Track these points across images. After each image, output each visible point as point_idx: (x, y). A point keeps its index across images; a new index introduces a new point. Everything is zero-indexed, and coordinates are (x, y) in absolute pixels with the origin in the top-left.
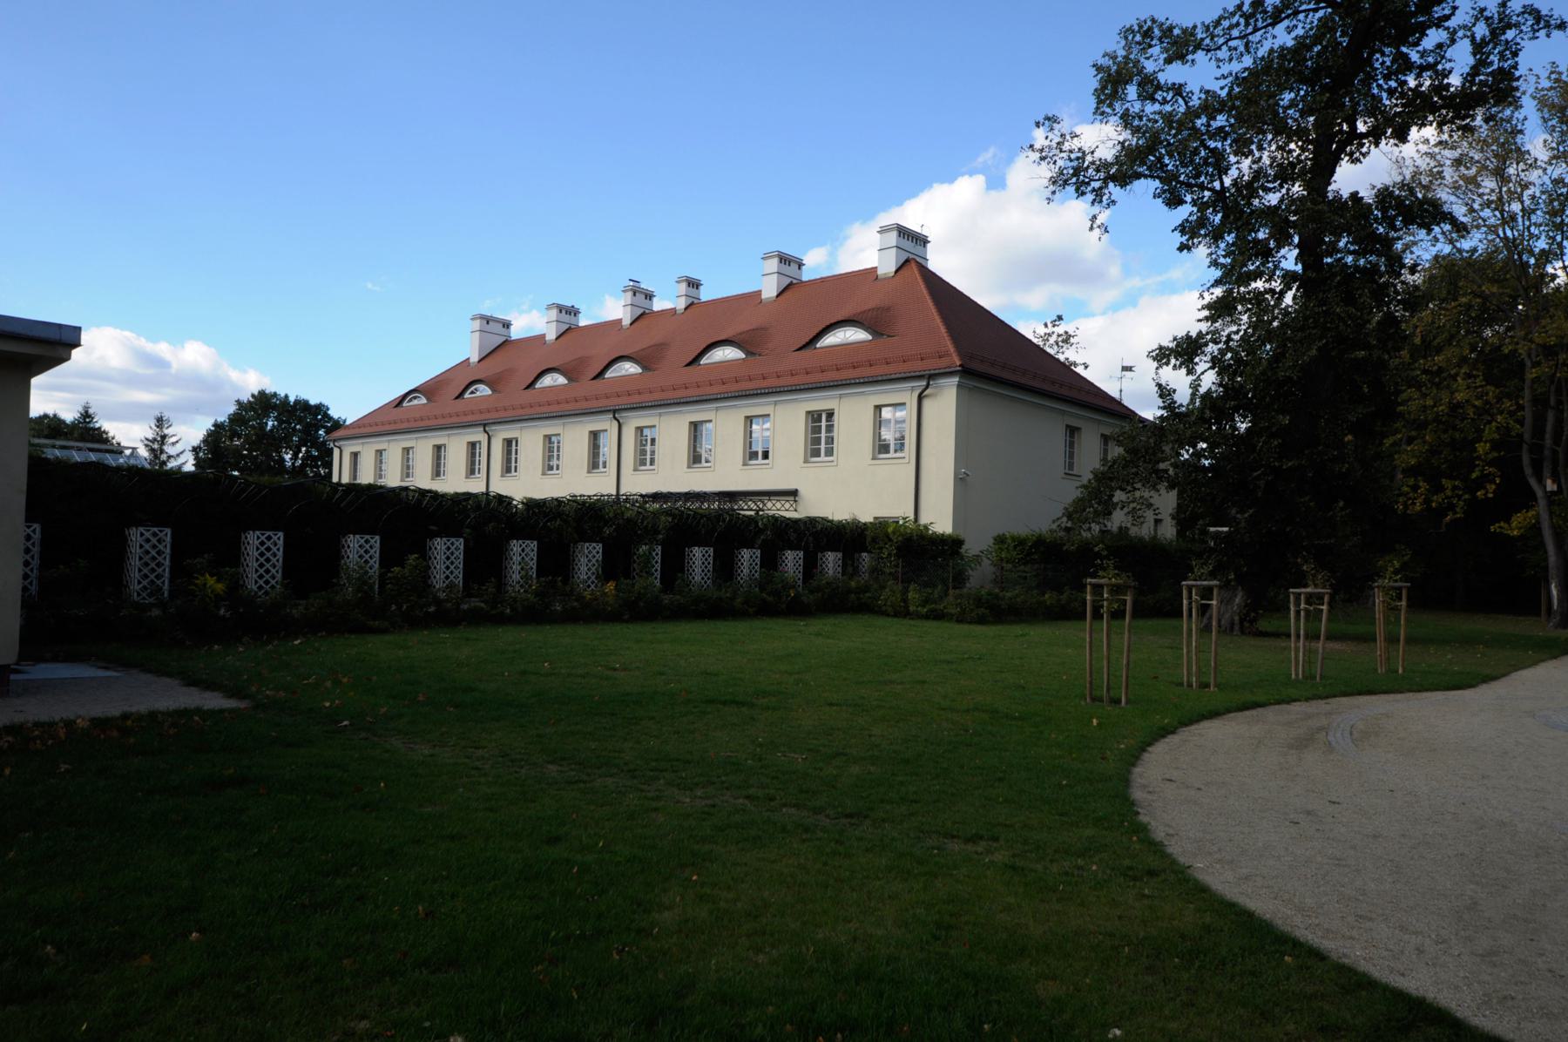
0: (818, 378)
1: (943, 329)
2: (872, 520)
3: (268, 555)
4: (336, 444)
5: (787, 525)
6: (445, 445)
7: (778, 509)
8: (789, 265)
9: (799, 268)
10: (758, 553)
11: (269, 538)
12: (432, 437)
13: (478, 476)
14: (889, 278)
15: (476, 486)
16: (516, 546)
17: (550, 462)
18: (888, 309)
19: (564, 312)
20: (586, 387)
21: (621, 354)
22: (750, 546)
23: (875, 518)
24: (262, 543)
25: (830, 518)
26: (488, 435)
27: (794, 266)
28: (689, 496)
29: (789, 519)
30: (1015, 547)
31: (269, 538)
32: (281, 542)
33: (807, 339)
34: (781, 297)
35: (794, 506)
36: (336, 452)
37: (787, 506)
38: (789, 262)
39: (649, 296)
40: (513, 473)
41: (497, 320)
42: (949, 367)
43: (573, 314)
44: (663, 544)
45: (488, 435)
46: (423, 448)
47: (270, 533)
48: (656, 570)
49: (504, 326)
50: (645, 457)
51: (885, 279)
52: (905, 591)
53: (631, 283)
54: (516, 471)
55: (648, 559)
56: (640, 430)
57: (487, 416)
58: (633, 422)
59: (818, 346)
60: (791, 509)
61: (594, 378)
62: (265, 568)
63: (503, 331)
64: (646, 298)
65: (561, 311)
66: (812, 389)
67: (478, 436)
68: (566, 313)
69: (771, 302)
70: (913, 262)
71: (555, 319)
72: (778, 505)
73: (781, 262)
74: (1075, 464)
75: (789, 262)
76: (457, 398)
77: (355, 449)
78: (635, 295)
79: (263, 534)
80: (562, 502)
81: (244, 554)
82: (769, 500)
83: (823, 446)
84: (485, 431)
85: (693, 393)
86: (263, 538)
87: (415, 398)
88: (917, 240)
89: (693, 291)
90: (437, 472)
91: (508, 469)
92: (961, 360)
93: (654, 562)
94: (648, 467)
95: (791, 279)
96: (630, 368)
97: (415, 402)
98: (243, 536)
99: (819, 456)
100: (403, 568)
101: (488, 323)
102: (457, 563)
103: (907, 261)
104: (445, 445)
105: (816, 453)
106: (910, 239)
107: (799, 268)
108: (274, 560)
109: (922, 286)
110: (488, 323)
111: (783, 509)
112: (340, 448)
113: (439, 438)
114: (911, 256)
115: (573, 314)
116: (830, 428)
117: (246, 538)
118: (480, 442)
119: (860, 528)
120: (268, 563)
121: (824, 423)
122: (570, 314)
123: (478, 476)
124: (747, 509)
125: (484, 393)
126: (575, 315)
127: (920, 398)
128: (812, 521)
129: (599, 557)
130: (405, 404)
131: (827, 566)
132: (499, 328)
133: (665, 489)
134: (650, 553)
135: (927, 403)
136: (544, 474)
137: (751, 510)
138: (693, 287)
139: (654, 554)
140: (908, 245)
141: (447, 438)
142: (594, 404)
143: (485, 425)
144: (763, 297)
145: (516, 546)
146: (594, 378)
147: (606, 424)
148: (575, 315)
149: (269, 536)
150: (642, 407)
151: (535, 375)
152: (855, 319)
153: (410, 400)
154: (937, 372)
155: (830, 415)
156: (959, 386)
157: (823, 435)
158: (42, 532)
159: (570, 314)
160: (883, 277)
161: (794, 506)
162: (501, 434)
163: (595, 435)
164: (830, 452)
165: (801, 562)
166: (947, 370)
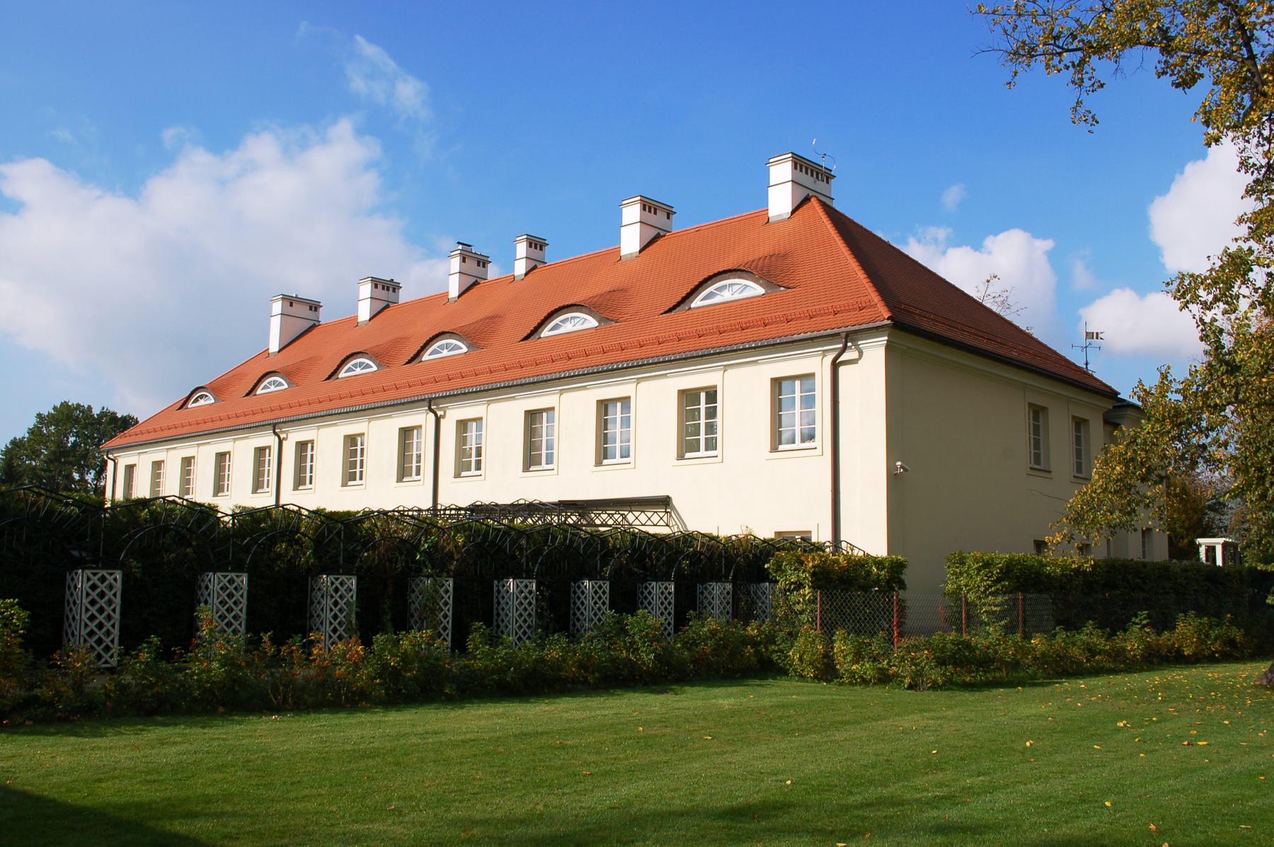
0: (712, 341)
1: (861, 275)
2: (772, 536)
3: (102, 602)
4: (110, 456)
5: (649, 543)
6: (312, 442)
7: (651, 524)
8: (655, 213)
9: (668, 218)
10: (606, 586)
11: (103, 579)
12: (594, 386)
13: (310, 486)
14: (783, 221)
15: (264, 500)
16: (215, 581)
17: (352, 472)
18: (785, 256)
19: (380, 287)
20: (400, 372)
21: (441, 331)
22: (718, 578)
23: (778, 533)
24: (94, 587)
25: (715, 534)
26: (436, 415)
27: (661, 216)
28: (515, 509)
29: (653, 536)
30: (979, 569)
31: (103, 579)
32: (119, 585)
33: (679, 299)
34: (797, 213)
35: (665, 518)
36: (110, 464)
37: (655, 518)
38: (655, 210)
39: (483, 262)
40: (308, 486)
41: (302, 301)
42: (874, 321)
43: (391, 289)
44: (457, 576)
45: (436, 415)
46: (204, 454)
47: (104, 572)
48: (445, 616)
49: (311, 309)
50: (468, 461)
51: (778, 222)
52: (830, 643)
53: (460, 247)
54: (311, 483)
55: (434, 598)
56: (462, 425)
57: (278, 413)
58: (454, 414)
59: (693, 305)
60: (661, 523)
61: (409, 362)
62: (97, 622)
63: (311, 314)
64: (479, 265)
65: (376, 286)
66: (685, 359)
67: (268, 439)
68: (383, 289)
69: (632, 258)
70: (813, 199)
71: (790, 179)
72: (643, 518)
73: (644, 209)
74: (1041, 441)
75: (655, 210)
76: (248, 395)
77: (130, 461)
78: (464, 260)
79: (95, 574)
80: (392, 517)
81: (69, 603)
82: (631, 511)
83: (702, 437)
84: (275, 433)
85: (530, 374)
86: (95, 579)
87: (201, 397)
88: (817, 174)
89: (536, 253)
90: (219, 488)
91: (299, 482)
92: (890, 310)
93: (441, 604)
94: (358, 482)
95: (657, 231)
96: (581, 322)
97: (202, 402)
98: (69, 578)
99: (355, 480)
100: (573, 637)
101: (291, 305)
102: (236, 610)
103: (806, 200)
104: (312, 442)
105: (694, 447)
106: (809, 171)
107: (668, 218)
108: (236, 624)
109: (829, 227)
110: (291, 305)
111: (649, 523)
112: (114, 460)
113: (222, 445)
114: (811, 193)
115: (391, 289)
116: (712, 413)
117: (73, 579)
118: (269, 447)
119: (757, 546)
120: (236, 621)
121: (703, 406)
122: (388, 289)
123: (267, 490)
124: (604, 521)
125: (586, 326)
126: (394, 291)
127: (835, 366)
128: (688, 538)
129: (352, 597)
130: (190, 405)
131: (710, 603)
132: (303, 311)
133: (487, 500)
134: (436, 591)
135: (842, 370)
136: (344, 484)
137: (606, 525)
138: (536, 248)
139: (442, 591)
140: (807, 179)
141: (165, 453)
142: (406, 394)
143: (274, 426)
144: (770, 215)
145: (215, 581)
146: (409, 362)
147: (421, 418)
148: (394, 291)
149: (103, 576)
150: (299, 420)
151: (338, 363)
152: (742, 268)
153: (196, 401)
154: (857, 328)
155: (712, 395)
156: (889, 349)
157: (703, 421)
158: (454, 584)
159: (388, 289)
160: (776, 219)
161: (665, 518)
162: (295, 435)
163: (406, 433)
164: (711, 445)
165: (672, 598)
166: (871, 325)
